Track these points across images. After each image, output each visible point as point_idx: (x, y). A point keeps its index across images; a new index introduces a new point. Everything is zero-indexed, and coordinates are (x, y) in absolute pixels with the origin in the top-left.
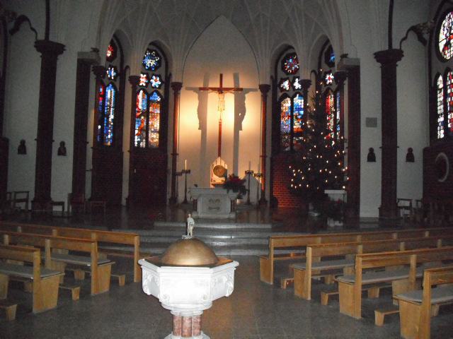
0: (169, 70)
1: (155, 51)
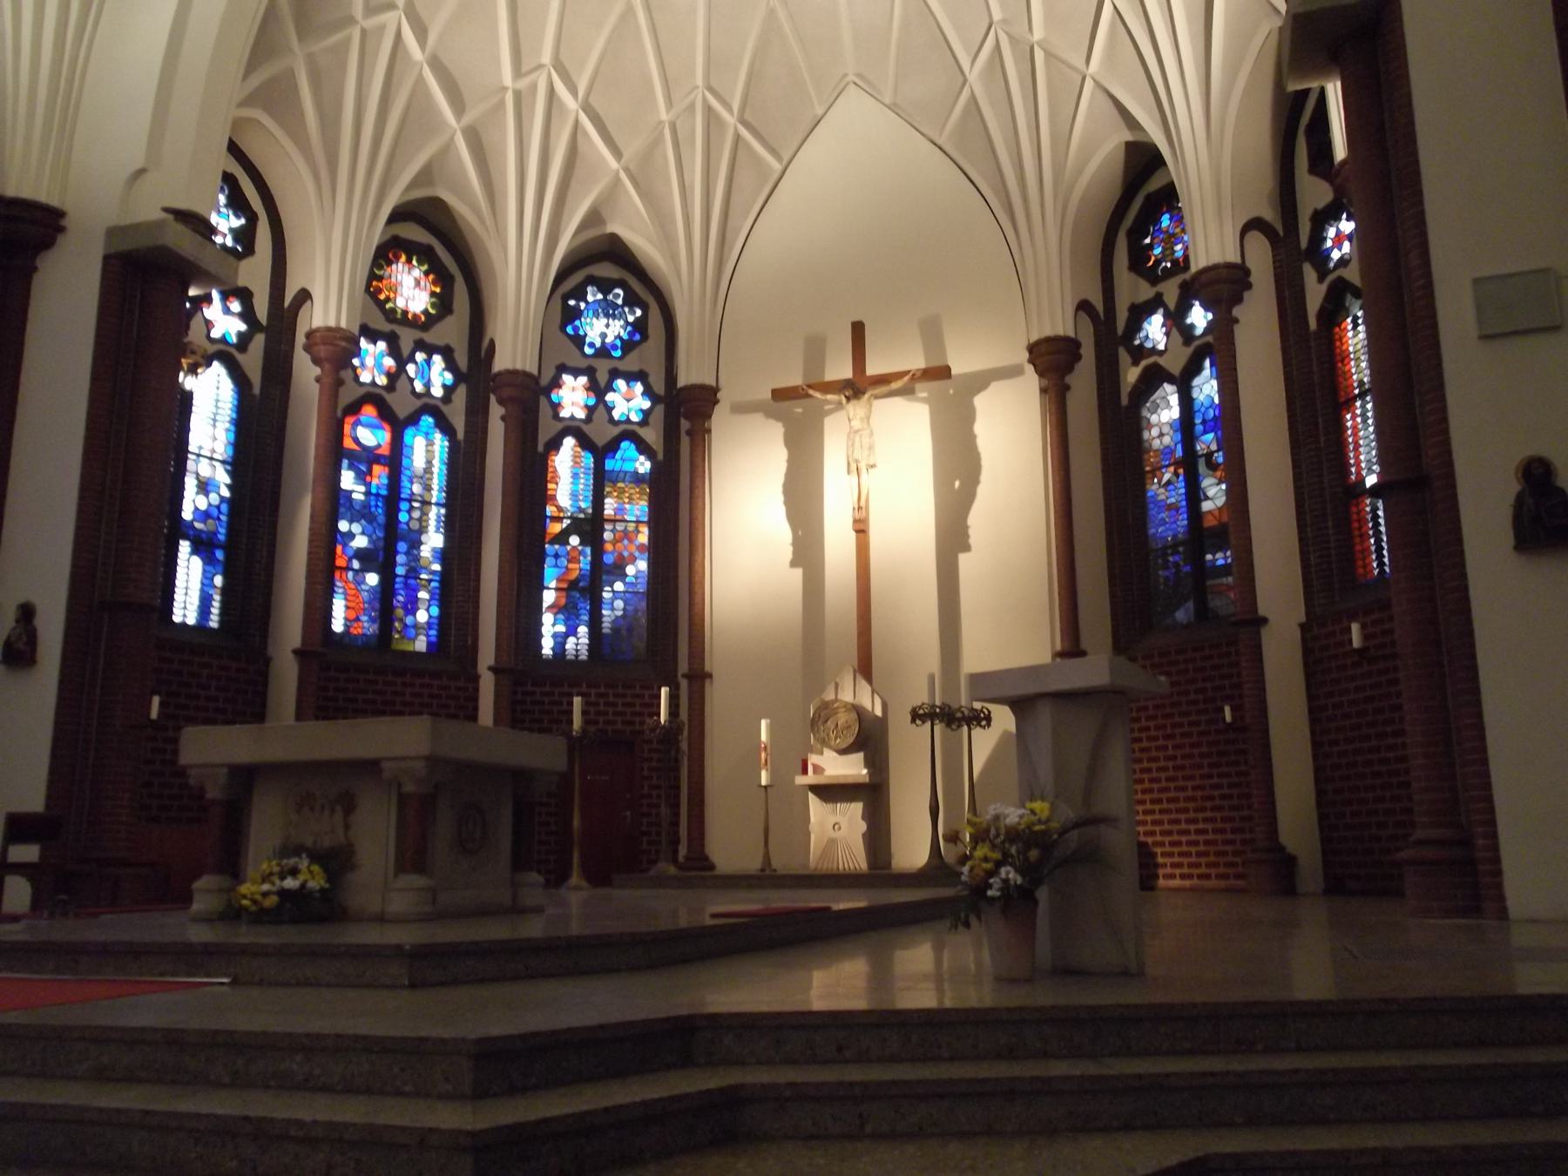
1: (621, 284)
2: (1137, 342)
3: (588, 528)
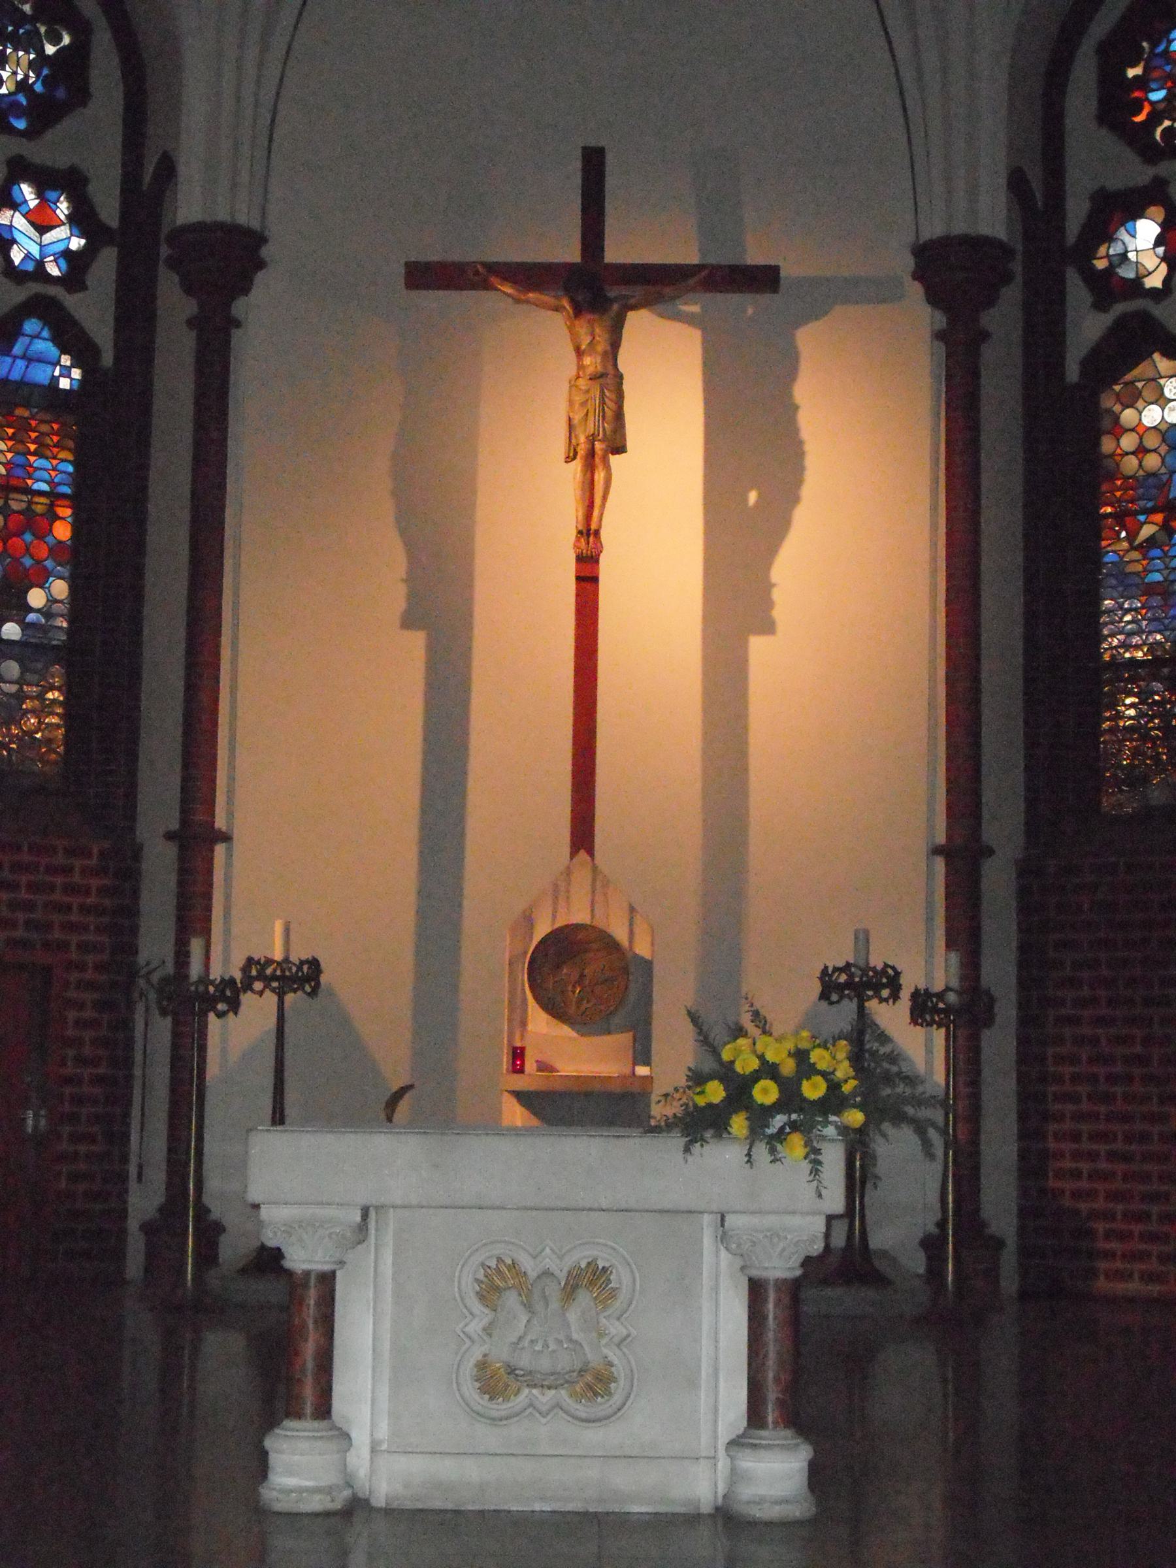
2: (1101, 264)
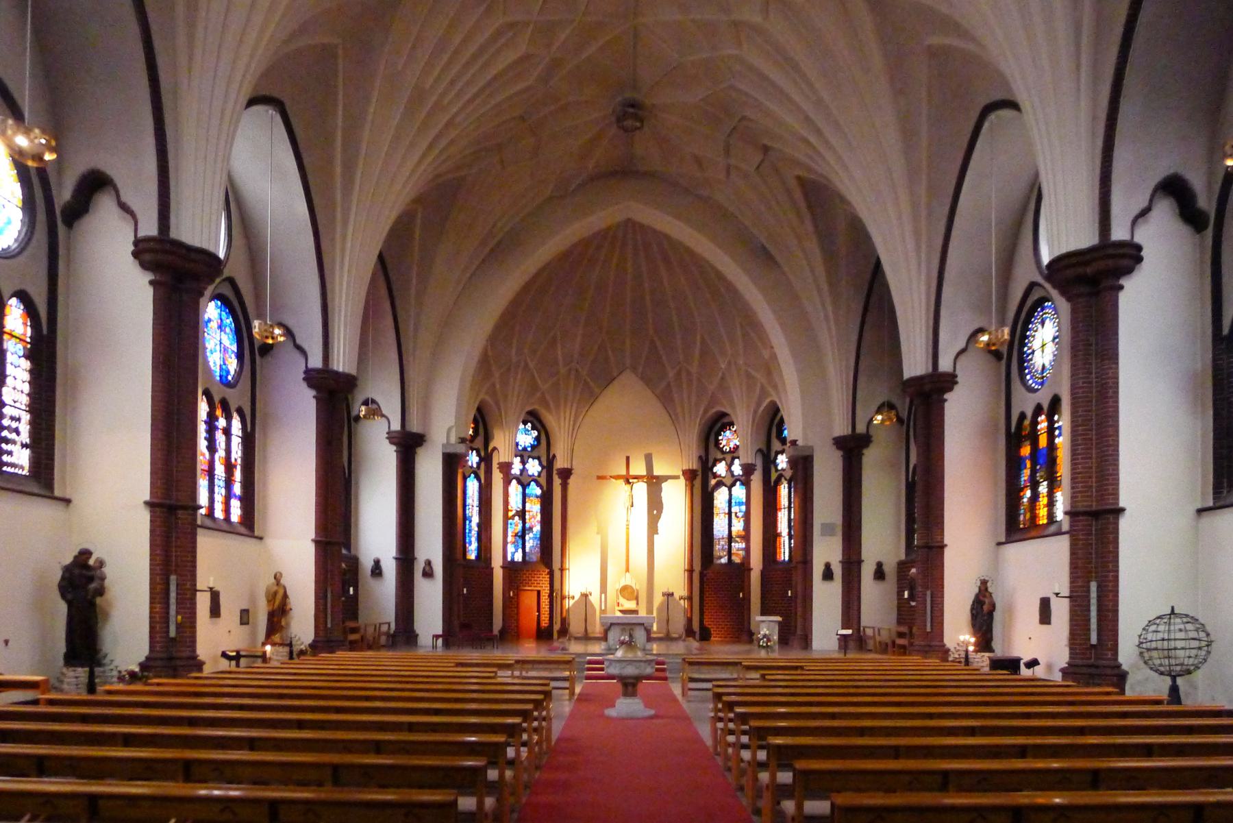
0: (552, 448)
3: (520, 514)
